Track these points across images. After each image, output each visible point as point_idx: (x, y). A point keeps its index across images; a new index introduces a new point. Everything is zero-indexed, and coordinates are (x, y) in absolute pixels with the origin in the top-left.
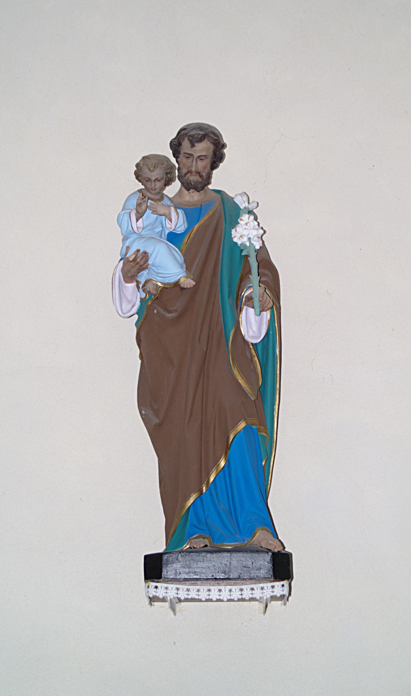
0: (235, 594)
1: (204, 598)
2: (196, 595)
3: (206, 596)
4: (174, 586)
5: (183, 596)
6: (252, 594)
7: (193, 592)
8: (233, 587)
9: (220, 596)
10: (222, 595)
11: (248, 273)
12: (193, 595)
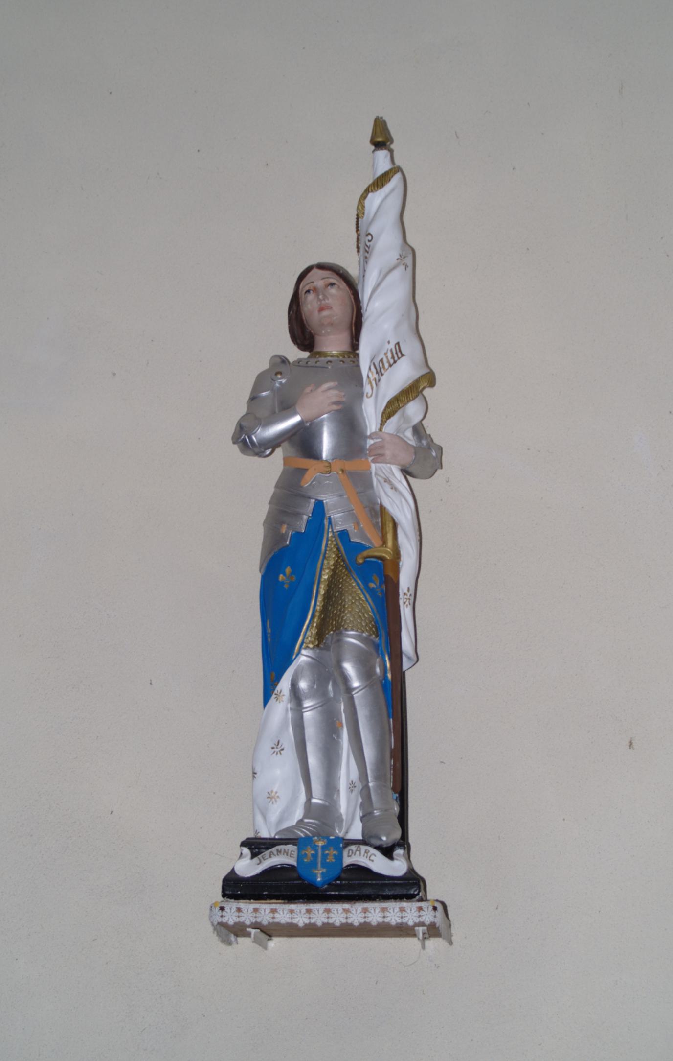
3: (234, 918)
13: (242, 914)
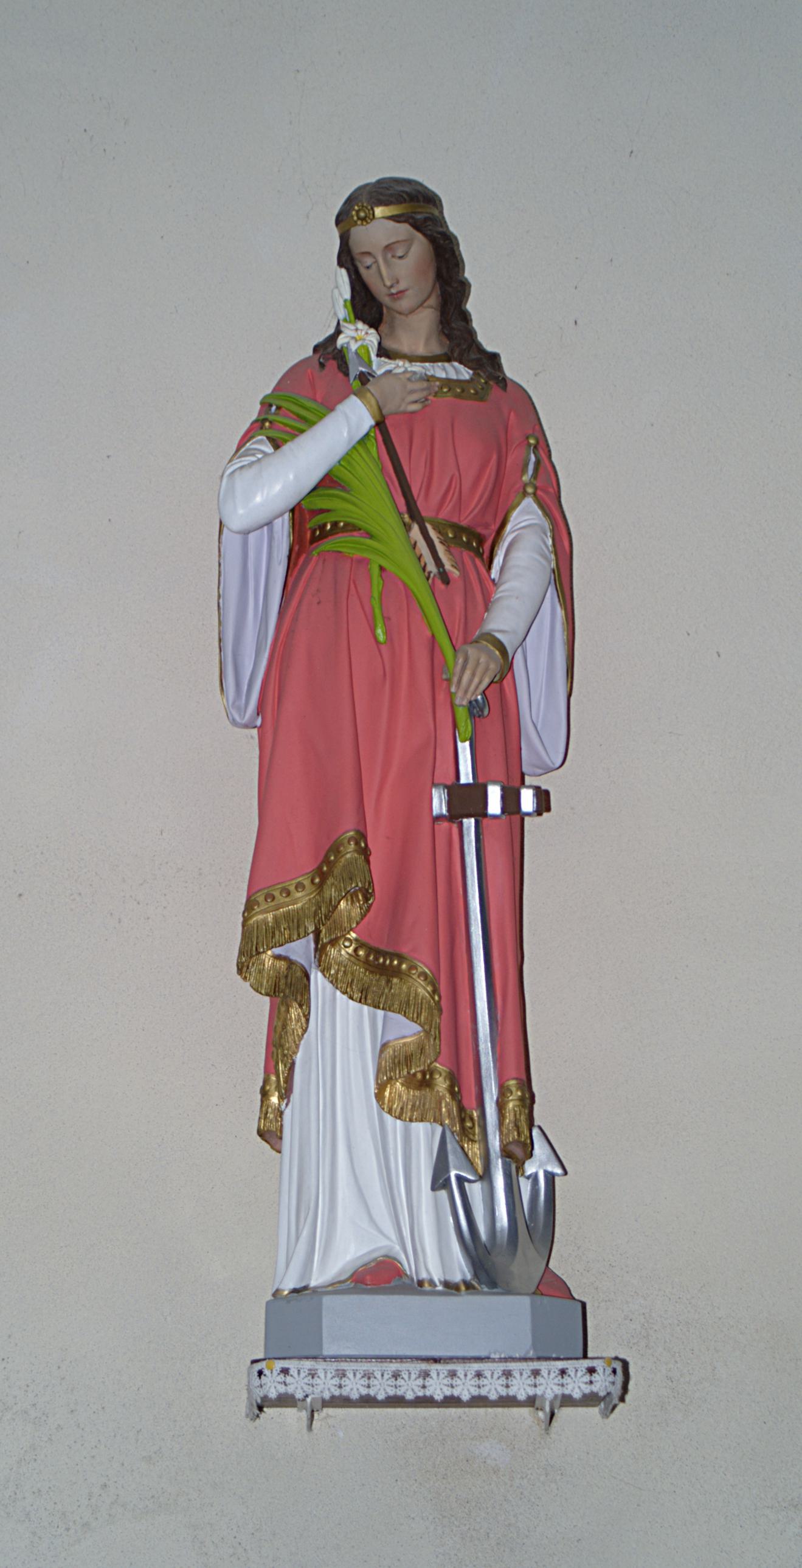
0: (464, 1384)
1: (383, 1393)
2: (555, 1384)
3: (583, 1386)
4: (498, 1367)
5: (577, 1390)
6: (452, 1386)
7: (466, 1379)
8: (485, 1366)
9: (535, 1386)
10: (345, 1386)
11: (462, 557)
12: (547, 1384)
13: (459, 1382)
